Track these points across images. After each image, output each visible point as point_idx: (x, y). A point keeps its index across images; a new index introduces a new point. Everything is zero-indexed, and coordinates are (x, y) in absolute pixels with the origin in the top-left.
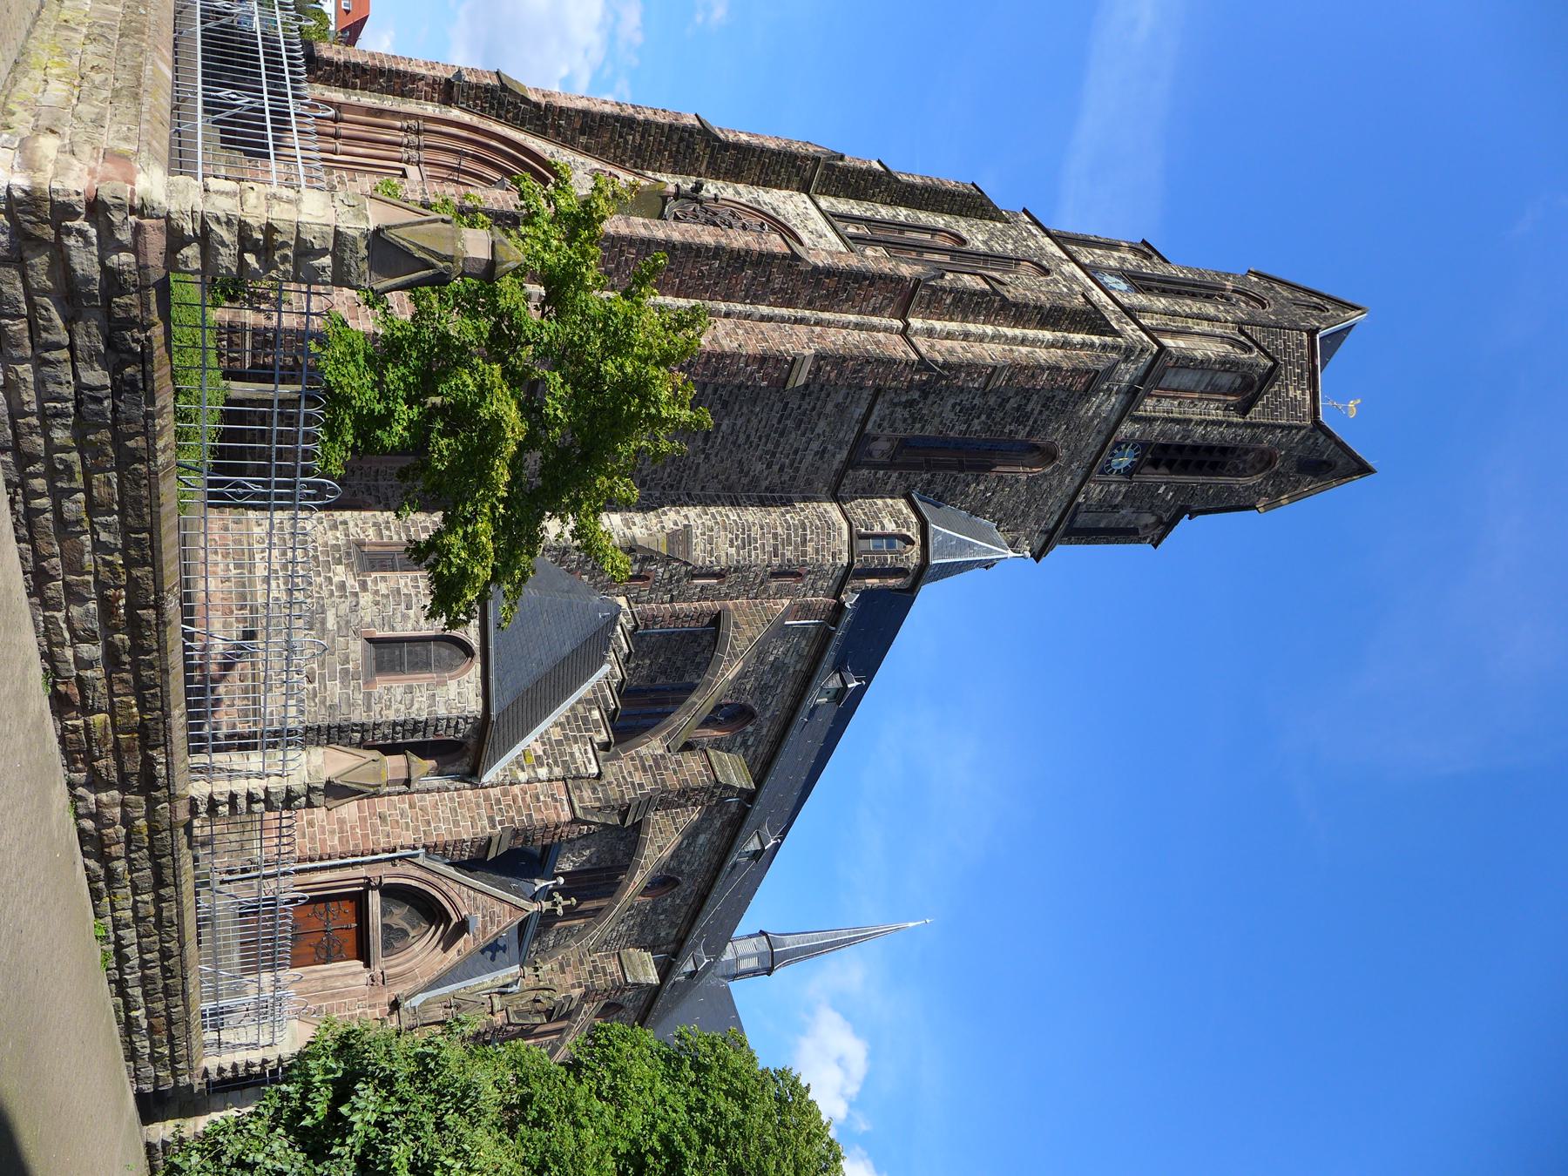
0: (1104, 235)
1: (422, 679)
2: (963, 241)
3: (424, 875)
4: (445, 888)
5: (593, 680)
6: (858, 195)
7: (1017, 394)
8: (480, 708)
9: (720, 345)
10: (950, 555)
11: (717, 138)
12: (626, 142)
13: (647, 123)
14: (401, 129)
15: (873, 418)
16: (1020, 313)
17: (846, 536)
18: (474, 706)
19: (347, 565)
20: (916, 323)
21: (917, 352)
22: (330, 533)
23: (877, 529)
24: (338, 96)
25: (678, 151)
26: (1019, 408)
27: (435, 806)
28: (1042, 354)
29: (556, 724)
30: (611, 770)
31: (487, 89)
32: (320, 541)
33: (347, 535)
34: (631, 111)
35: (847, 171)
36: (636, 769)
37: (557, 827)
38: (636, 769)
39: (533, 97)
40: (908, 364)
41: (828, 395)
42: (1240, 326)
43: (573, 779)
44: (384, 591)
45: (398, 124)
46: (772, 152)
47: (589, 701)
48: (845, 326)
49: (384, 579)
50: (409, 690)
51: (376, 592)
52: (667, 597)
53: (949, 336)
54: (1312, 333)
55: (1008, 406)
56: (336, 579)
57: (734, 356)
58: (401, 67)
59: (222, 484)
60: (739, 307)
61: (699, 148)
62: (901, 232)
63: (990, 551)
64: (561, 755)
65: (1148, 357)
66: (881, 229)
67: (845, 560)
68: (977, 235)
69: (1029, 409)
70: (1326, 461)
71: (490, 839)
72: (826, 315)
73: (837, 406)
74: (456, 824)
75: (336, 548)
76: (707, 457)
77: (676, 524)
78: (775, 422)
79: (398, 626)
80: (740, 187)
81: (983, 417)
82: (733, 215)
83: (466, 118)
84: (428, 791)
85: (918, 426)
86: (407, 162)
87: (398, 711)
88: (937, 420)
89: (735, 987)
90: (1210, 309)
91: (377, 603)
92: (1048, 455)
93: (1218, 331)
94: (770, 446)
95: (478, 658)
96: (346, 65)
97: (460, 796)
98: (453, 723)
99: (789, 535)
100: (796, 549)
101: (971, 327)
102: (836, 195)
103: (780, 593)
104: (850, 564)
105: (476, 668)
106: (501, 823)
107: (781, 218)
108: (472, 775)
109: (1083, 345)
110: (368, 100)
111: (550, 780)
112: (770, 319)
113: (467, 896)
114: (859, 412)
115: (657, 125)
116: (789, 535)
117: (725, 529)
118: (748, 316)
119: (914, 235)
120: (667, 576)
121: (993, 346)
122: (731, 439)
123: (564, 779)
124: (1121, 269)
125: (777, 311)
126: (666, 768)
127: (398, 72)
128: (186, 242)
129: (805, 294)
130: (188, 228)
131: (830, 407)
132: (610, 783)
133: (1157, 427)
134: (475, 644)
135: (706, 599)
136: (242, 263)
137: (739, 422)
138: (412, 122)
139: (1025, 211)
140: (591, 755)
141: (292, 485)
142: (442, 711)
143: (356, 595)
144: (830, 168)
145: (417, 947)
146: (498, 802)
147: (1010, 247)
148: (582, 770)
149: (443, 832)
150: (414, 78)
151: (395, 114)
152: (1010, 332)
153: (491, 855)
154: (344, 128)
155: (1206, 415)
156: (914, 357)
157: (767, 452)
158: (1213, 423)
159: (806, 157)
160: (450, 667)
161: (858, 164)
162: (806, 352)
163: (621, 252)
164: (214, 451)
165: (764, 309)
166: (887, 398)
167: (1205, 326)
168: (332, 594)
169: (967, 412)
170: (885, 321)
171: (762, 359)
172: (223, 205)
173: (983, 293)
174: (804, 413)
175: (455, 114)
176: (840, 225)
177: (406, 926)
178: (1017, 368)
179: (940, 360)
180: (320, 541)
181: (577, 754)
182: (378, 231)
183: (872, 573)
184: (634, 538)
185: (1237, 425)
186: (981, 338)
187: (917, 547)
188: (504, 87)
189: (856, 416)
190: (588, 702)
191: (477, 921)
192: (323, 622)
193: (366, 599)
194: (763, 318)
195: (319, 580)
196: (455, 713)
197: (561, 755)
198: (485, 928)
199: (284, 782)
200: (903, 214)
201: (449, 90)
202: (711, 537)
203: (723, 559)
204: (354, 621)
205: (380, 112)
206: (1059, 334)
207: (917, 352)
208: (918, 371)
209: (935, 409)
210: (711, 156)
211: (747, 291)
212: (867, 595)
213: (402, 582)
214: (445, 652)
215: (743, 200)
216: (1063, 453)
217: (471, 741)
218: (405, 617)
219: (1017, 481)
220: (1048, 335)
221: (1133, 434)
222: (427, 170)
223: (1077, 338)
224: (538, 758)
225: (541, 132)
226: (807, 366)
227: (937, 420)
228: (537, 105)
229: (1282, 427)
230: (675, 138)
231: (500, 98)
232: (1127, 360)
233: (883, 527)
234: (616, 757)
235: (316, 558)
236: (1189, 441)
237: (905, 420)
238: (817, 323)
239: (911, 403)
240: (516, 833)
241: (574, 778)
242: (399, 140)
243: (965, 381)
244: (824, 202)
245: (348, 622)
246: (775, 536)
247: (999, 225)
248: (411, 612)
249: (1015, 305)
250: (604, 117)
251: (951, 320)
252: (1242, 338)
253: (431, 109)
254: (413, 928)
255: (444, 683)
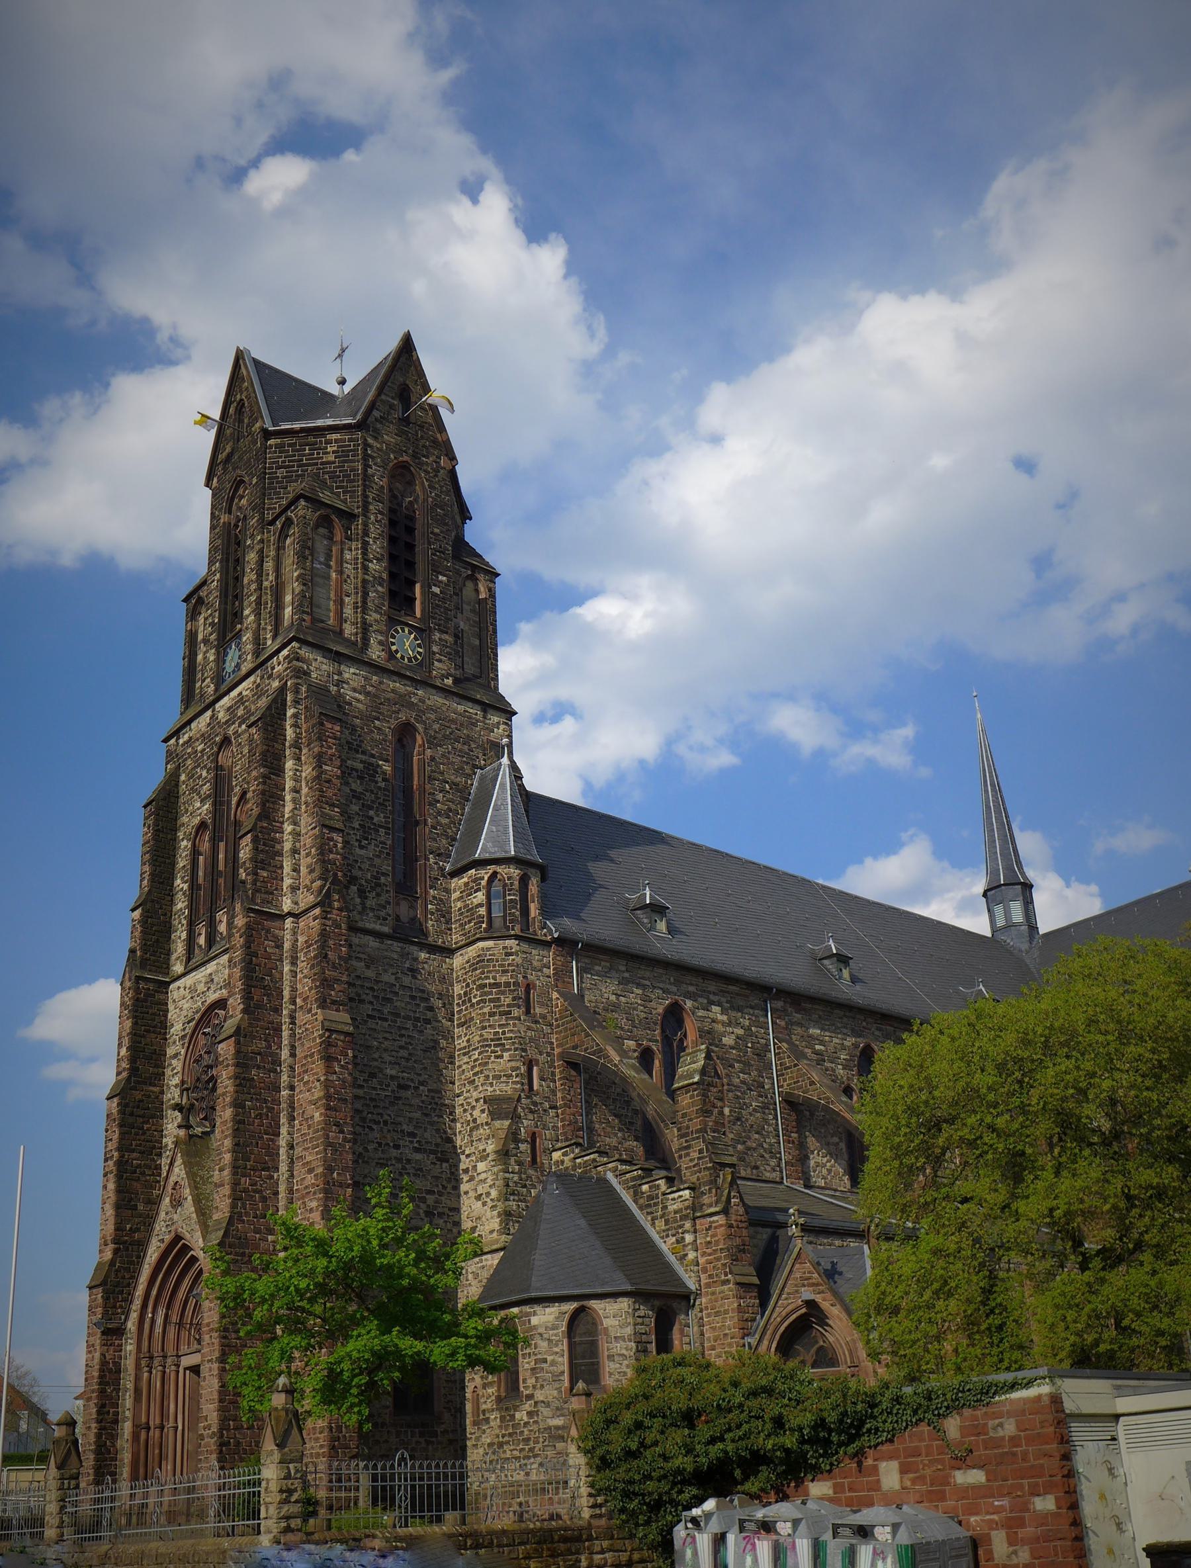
0: (180, 649)
1: (604, 1347)
2: (202, 825)
3: (768, 1337)
4: (779, 1319)
5: (618, 1188)
6: (167, 930)
7: (347, 784)
8: (626, 1299)
9: (320, 1099)
10: (506, 833)
11: (128, 1079)
12: (139, 1166)
13: (119, 1149)
14: (150, 1372)
15: (378, 927)
16: (271, 797)
17: (490, 943)
18: (624, 1304)
19: (515, 1410)
20: (287, 905)
21: (313, 907)
22: (492, 1424)
23: (483, 911)
24: (127, 1428)
25: (143, 1116)
26: (361, 778)
27: (714, 1329)
28: (307, 771)
29: (653, 1224)
30: (690, 1177)
31: (106, 1299)
32: (497, 1431)
33: (493, 1410)
34: (110, 1163)
35: (145, 947)
36: (688, 1155)
37: (731, 1226)
38: (688, 1155)
39: (108, 1255)
40: (324, 916)
41: (358, 977)
42: (265, 524)
43: (694, 1211)
44: (533, 1380)
45: (146, 1375)
46: (135, 1024)
47: (636, 1194)
48: (294, 974)
49: (524, 1381)
50: (611, 1358)
51: (534, 1387)
52: (552, 1113)
53: (296, 870)
54: (267, 434)
55: (359, 790)
56: (525, 1418)
57: (327, 1085)
58: (96, 1374)
59: (400, 1507)
60: (284, 1078)
61: (138, 1095)
62: (199, 887)
63: (503, 785)
64: (675, 1221)
65: (305, 652)
66: (197, 910)
67: (512, 943)
68: (196, 810)
69: (360, 766)
70: (403, 369)
71: (738, 1284)
72: (286, 993)
73: (368, 967)
74: (726, 1312)
75: (502, 1418)
76: (422, 1083)
77: (483, 1111)
78: (386, 1024)
79: (561, 1368)
80: (170, 1051)
81: (371, 813)
82: (197, 1061)
83: (134, 1316)
84: (702, 1334)
85: (383, 879)
86: (178, 1366)
87: (628, 1366)
88: (377, 861)
89: (1043, 928)
90: (252, 556)
91: (542, 1386)
92: (405, 732)
93: (272, 553)
94: (409, 1025)
95: (585, 1303)
96: (99, 1421)
97: (707, 1308)
98: (640, 1320)
99: (491, 1001)
100: (503, 993)
101: (287, 846)
102: (169, 953)
103: (547, 1003)
104: (516, 937)
105: (594, 1304)
106: (726, 1275)
107: (197, 1017)
108: (686, 1299)
109: (295, 725)
110: (128, 1401)
111: (695, 1232)
112: (293, 1047)
113: (787, 1303)
114: (372, 942)
115: (121, 1139)
116: (491, 1001)
117: (487, 1063)
118: (292, 1068)
119: (201, 873)
120: (531, 1116)
121: (303, 823)
122: (404, 1063)
123: (694, 1219)
124: (218, 647)
125: (285, 1042)
126: (688, 1127)
127: (101, 1377)
128: (289, 1526)
129: (273, 1016)
130: (284, 1524)
131: (370, 973)
132: (698, 1179)
133: (373, 616)
134: (571, 1306)
135: (553, 1074)
136: (296, 1502)
137: (387, 1058)
138: (143, 1363)
139: (166, 741)
140: (676, 1195)
141: (400, 1474)
142: (629, 1330)
143: (536, 1403)
144: (144, 964)
145: (831, 1339)
146: (710, 1276)
147: (204, 774)
148: (686, 1203)
149: (731, 1322)
150: (104, 1363)
151: (138, 1378)
152: (289, 807)
153: (756, 1280)
154: (155, 1420)
155: (360, 559)
156: (317, 911)
157: (415, 1026)
158: (365, 553)
159: (137, 990)
160: (595, 1324)
161: (137, 934)
162: (320, 1018)
163: (245, 1191)
164: (384, 1509)
165: (285, 1053)
166: (358, 917)
167: (269, 565)
168: (536, 1422)
169: (367, 831)
170: (288, 936)
171: (328, 1059)
172: (272, 1510)
173: (255, 840)
174: (376, 997)
175: (131, 1325)
176: (198, 957)
177: (815, 1348)
178: (321, 801)
179: (319, 883)
180: (497, 1431)
181: (675, 1207)
182: (277, 1445)
183: (525, 911)
184: (496, 1152)
185: (365, 525)
186: (296, 835)
187: (499, 869)
188: (103, 1283)
189: (377, 944)
190: (637, 1195)
191: (807, 1294)
192: (557, 1428)
193: (539, 1395)
194: (293, 1055)
195: (526, 1433)
196: (630, 1320)
197: (675, 1221)
198: (813, 1285)
199: (583, 1467)
200: (181, 884)
201: (111, 1332)
202: (494, 1077)
203: (513, 1064)
204: (557, 1404)
205: (137, 1391)
206: (288, 752)
207: (313, 907)
208: (330, 906)
209: (366, 866)
210: (145, 1083)
211: (270, 1071)
212: (546, 912)
213: (527, 1366)
214: (581, 1329)
215: (183, 1052)
216: (403, 717)
217: (657, 1303)
218: (553, 1363)
219: (433, 759)
220: (289, 764)
221: (380, 643)
222: (184, 1349)
223: (290, 733)
224: (678, 1242)
225: (142, 1245)
226: (333, 1014)
227: (377, 861)
228: (116, 1252)
229: (366, 466)
230: (131, 1120)
231: (113, 1286)
232: (307, 674)
233: (480, 905)
234: (679, 1170)
235: (510, 1435)
236: (385, 576)
237: (378, 895)
238: (294, 1003)
239: (362, 893)
240: (735, 1260)
241: (694, 1210)
242: (159, 1374)
243: (337, 853)
244: (178, 968)
245: (557, 1409)
246: (492, 1014)
247: (183, 777)
248: (549, 1358)
249: (263, 805)
250: (119, 1191)
251: (282, 867)
252: (279, 524)
253: (130, 1347)
254: (817, 1342)
255: (606, 1329)
